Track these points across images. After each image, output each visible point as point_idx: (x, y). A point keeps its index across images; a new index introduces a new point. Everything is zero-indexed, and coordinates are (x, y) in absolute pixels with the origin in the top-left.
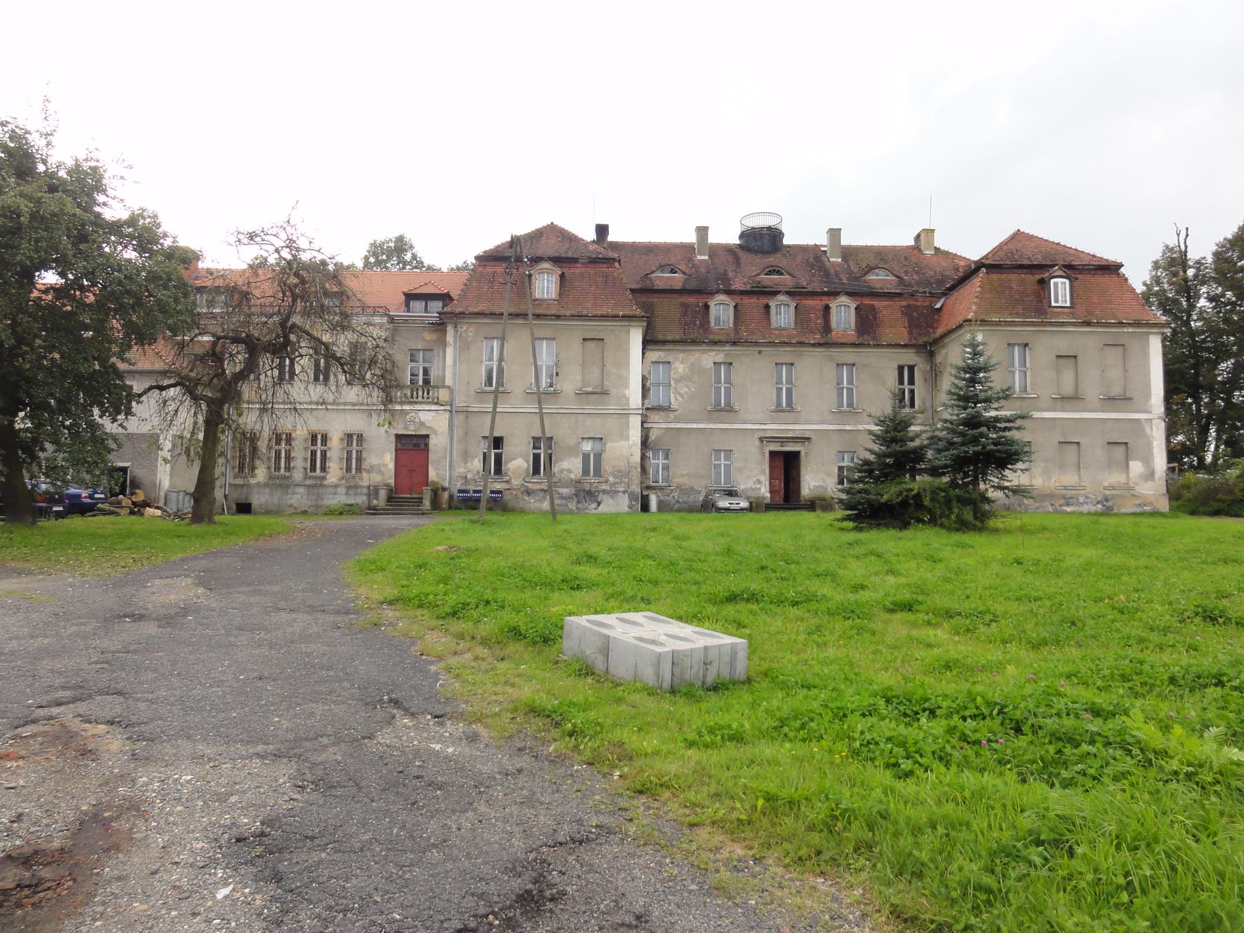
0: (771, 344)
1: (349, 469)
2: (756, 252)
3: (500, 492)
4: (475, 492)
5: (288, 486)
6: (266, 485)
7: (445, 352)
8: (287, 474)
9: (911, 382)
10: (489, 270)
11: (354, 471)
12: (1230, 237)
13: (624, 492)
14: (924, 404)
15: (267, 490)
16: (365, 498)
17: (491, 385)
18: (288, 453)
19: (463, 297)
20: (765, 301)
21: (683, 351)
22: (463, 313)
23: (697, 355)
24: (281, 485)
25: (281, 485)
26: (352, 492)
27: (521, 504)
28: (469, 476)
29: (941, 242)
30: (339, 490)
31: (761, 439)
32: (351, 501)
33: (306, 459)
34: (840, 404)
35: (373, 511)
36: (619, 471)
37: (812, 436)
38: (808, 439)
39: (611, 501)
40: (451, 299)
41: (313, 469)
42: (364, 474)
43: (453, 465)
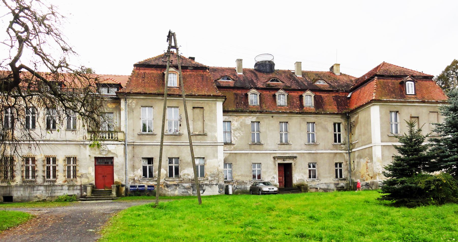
0: (278, 113)
1: (69, 176)
2: (264, 72)
3: (153, 186)
4: (139, 186)
5: (34, 187)
6: (21, 186)
7: (120, 114)
8: (33, 180)
9: (339, 131)
10: (142, 71)
11: (72, 177)
12: (439, 75)
13: (216, 185)
14: (345, 140)
15: (22, 189)
16: (78, 192)
17: (146, 131)
18: (33, 168)
19: (128, 85)
20: (273, 93)
21: (237, 116)
22: (129, 93)
23: (243, 118)
24: (30, 186)
25: (30, 186)
26: (71, 188)
27: (164, 192)
28: (136, 178)
29: (343, 70)
30: (64, 187)
31: (274, 158)
32: (71, 193)
33: (44, 171)
34: (309, 141)
35: (84, 198)
36: (213, 174)
37: (297, 156)
38: (296, 157)
39: (210, 189)
40: (122, 87)
41: (48, 176)
42: (78, 179)
43: (126, 173)
